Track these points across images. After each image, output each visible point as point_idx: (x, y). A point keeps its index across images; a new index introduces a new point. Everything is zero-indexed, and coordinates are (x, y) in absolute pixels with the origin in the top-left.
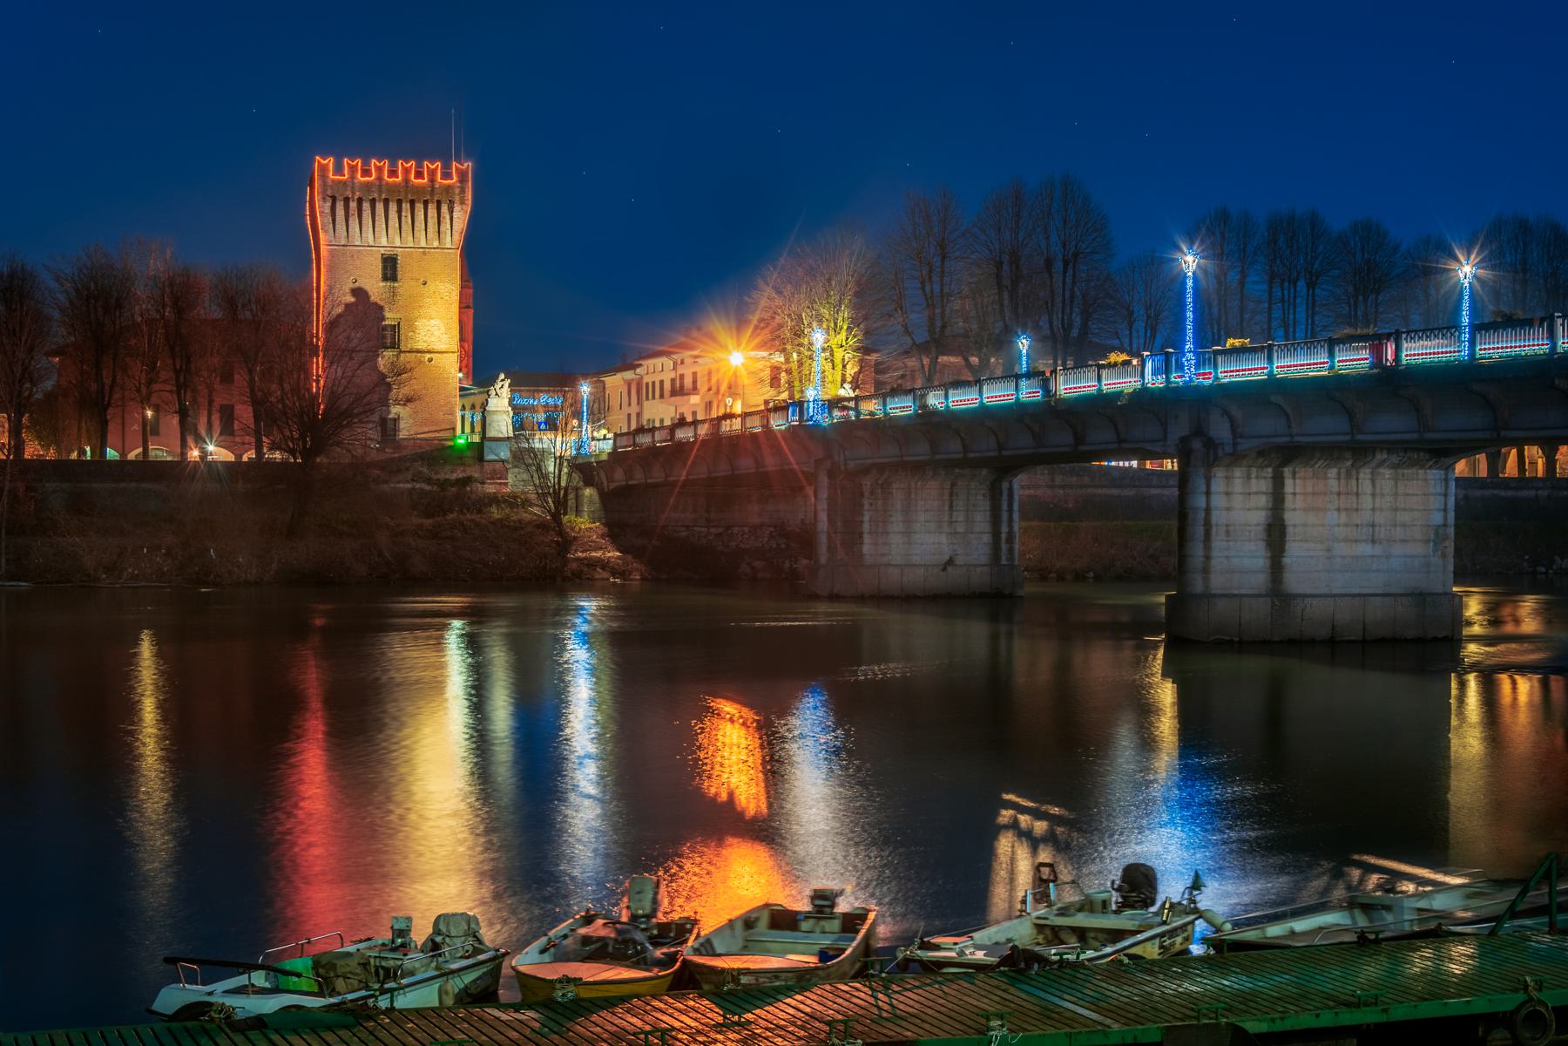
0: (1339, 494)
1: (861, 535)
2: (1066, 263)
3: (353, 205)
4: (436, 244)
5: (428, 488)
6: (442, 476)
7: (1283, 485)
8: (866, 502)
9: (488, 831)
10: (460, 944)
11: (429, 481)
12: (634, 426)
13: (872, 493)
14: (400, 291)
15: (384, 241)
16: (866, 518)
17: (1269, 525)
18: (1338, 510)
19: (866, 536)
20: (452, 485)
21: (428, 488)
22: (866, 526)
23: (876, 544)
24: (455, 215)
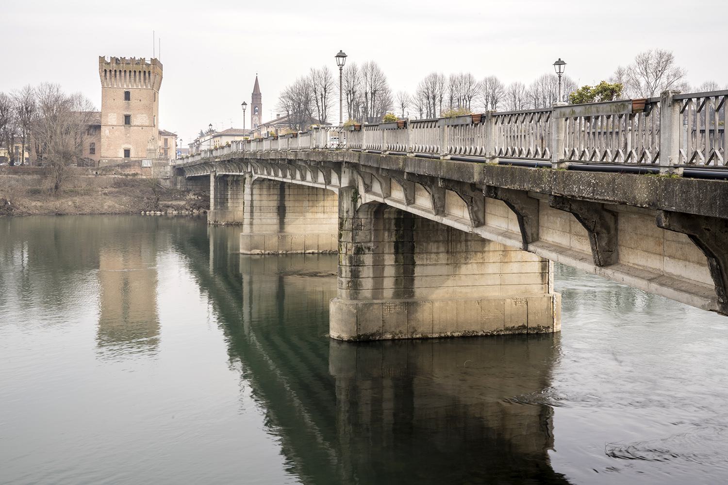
0: (309, 195)
1: (227, 199)
2: (372, 93)
3: (113, 73)
4: (144, 87)
5: (120, 177)
6: (126, 173)
7: (284, 191)
8: (229, 188)
9: (157, 316)
10: (551, 365)
11: (121, 174)
12: (369, 128)
13: (231, 184)
14: (131, 104)
15: (125, 87)
16: (229, 193)
17: (279, 207)
18: (309, 201)
19: (229, 200)
20: (130, 175)
21: (120, 177)
22: (229, 196)
23: (233, 203)
24: (151, 77)
